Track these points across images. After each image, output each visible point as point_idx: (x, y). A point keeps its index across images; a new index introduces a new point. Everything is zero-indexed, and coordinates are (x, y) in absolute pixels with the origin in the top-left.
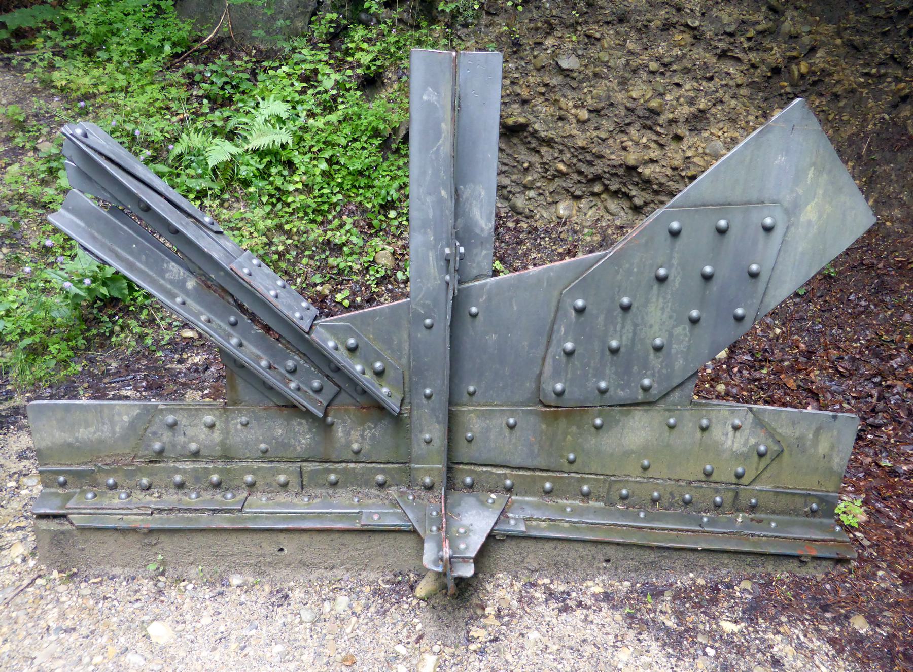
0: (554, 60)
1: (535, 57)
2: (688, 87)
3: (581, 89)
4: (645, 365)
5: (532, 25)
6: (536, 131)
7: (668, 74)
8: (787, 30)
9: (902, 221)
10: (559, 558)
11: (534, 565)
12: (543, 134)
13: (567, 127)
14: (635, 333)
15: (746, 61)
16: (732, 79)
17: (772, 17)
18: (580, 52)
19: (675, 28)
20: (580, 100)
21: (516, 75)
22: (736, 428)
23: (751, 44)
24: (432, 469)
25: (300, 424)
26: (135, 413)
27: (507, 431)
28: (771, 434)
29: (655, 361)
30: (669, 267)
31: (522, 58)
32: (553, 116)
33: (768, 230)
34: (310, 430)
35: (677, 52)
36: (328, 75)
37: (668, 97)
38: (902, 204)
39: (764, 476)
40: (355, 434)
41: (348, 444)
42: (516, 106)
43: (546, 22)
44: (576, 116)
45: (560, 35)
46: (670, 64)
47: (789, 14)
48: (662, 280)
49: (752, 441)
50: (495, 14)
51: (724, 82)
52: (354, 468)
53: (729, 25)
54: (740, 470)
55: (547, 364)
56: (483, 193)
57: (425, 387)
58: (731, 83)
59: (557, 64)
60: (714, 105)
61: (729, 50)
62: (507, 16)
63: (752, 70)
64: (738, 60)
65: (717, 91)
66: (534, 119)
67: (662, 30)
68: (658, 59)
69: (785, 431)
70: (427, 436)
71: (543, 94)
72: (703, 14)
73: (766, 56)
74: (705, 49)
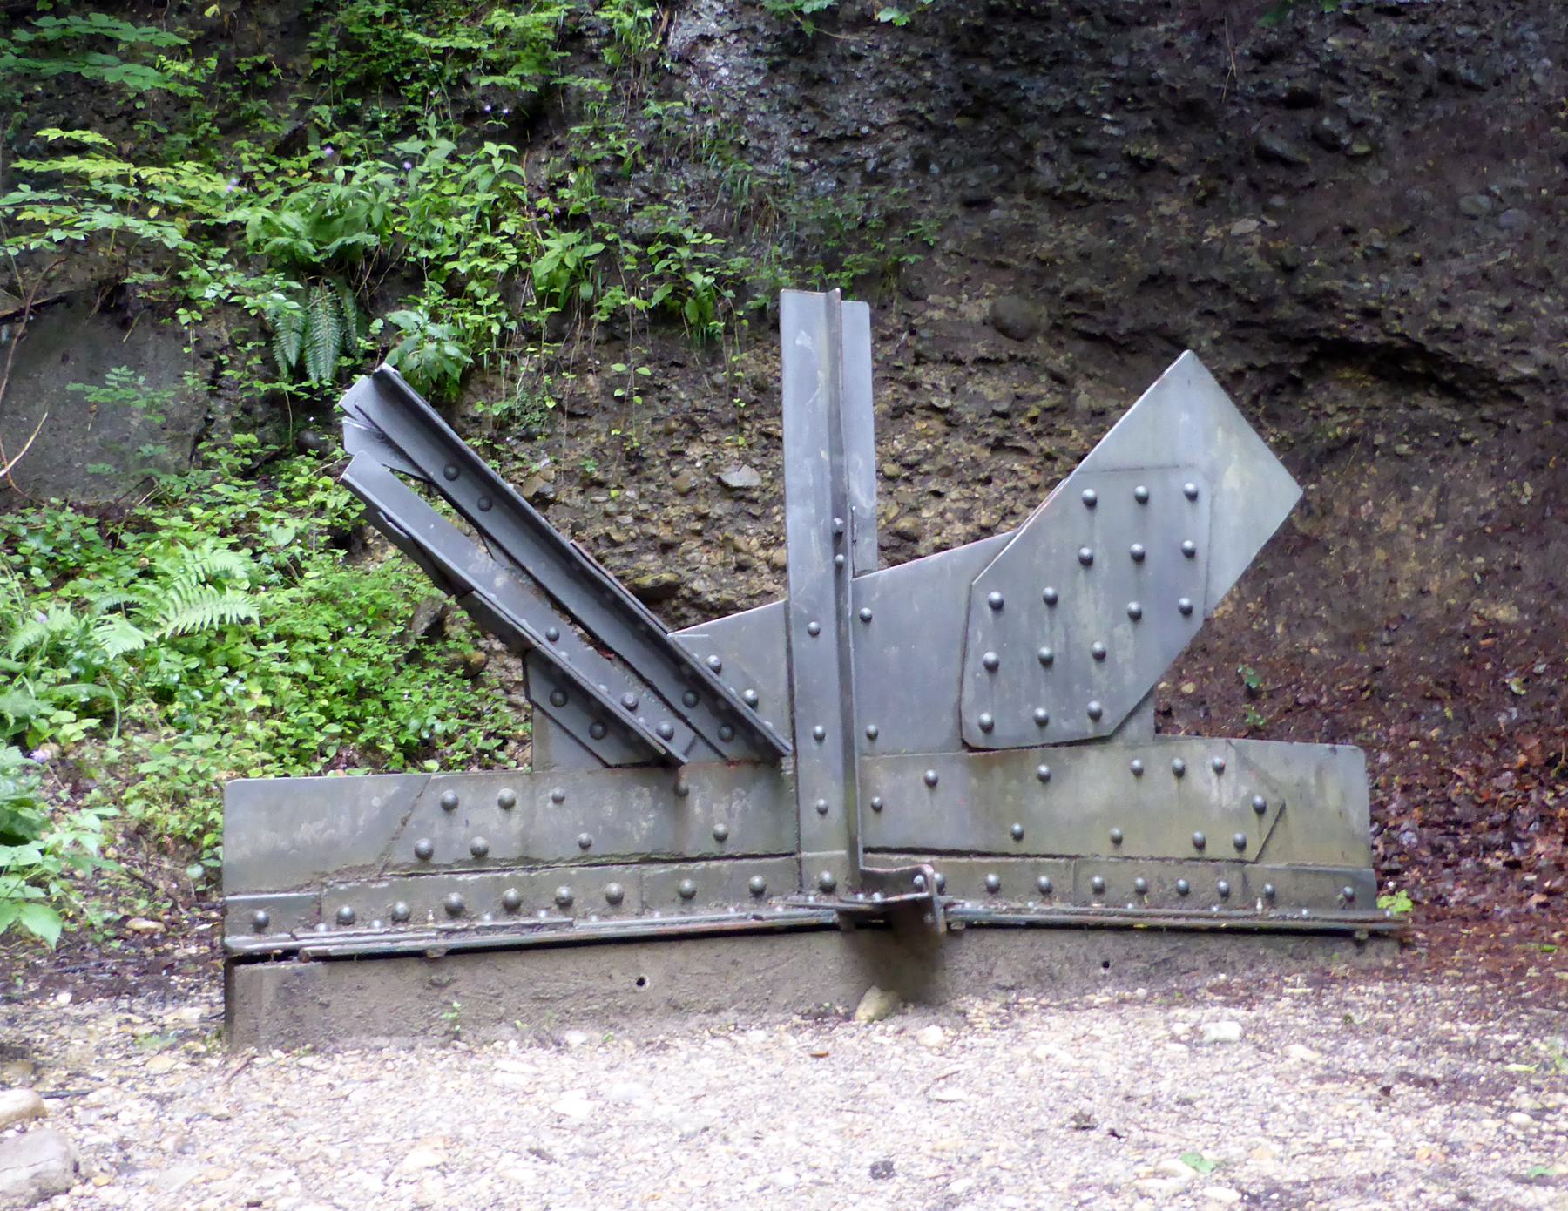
0: (712, 476)
1: (674, 475)
2: (954, 495)
3: (769, 517)
4: (1088, 682)
5: (659, 428)
6: (696, 594)
7: (916, 479)
8: (1085, 405)
9: (1331, 645)
10: (1040, 963)
11: (1008, 980)
12: (711, 598)
13: (754, 580)
14: (1067, 636)
15: (1035, 451)
16: (1021, 479)
17: (1058, 388)
18: (756, 461)
19: (912, 413)
20: (770, 534)
21: (642, 507)
22: (1219, 770)
23: (1039, 426)
24: (832, 858)
25: (640, 796)
26: (393, 791)
27: (925, 790)
28: (1264, 779)
29: (1097, 673)
30: (1092, 546)
31: (649, 480)
32: (723, 565)
33: (1192, 497)
34: (655, 805)
35: (922, 445)
36: (282, 524)
37: (925, 514)
38: (1324, 625)
39: (1272, 847)
40: (719, 809)
41: (710, 823)
42: (650, 557)
43: (685, 420)
44: (768, 561)
45: (714, 438)
46: (918, 463)
47: (1081, 385)
48: (1087, 562)
49: (1244, 790)
50: (584, 416)
51: (1009, 484)
52: (719, 868)
53: (997, 401)
54: (1239, 837)
55: (966, 685)
56: (861, 463)
57: (816, 724)
58: (1020, 484)
59: (720, 481)
60: (1003, 519)
61: (1005, 438)
62: (607, 417)
63: (1048, 464)
64: (1023, 452)
65: (1002, 499)
66: (690, 575)
67: (893, 418)
68: (896, 459)
69: (1279, 774)
70: (822, 803)
71: (698, 533)
72: (953, 390)
73: (1063, 442)
74: (968, 439)
